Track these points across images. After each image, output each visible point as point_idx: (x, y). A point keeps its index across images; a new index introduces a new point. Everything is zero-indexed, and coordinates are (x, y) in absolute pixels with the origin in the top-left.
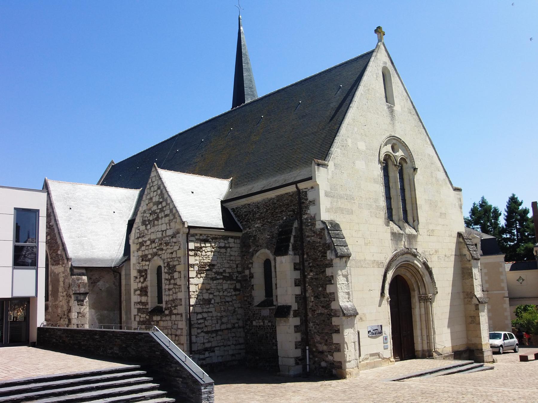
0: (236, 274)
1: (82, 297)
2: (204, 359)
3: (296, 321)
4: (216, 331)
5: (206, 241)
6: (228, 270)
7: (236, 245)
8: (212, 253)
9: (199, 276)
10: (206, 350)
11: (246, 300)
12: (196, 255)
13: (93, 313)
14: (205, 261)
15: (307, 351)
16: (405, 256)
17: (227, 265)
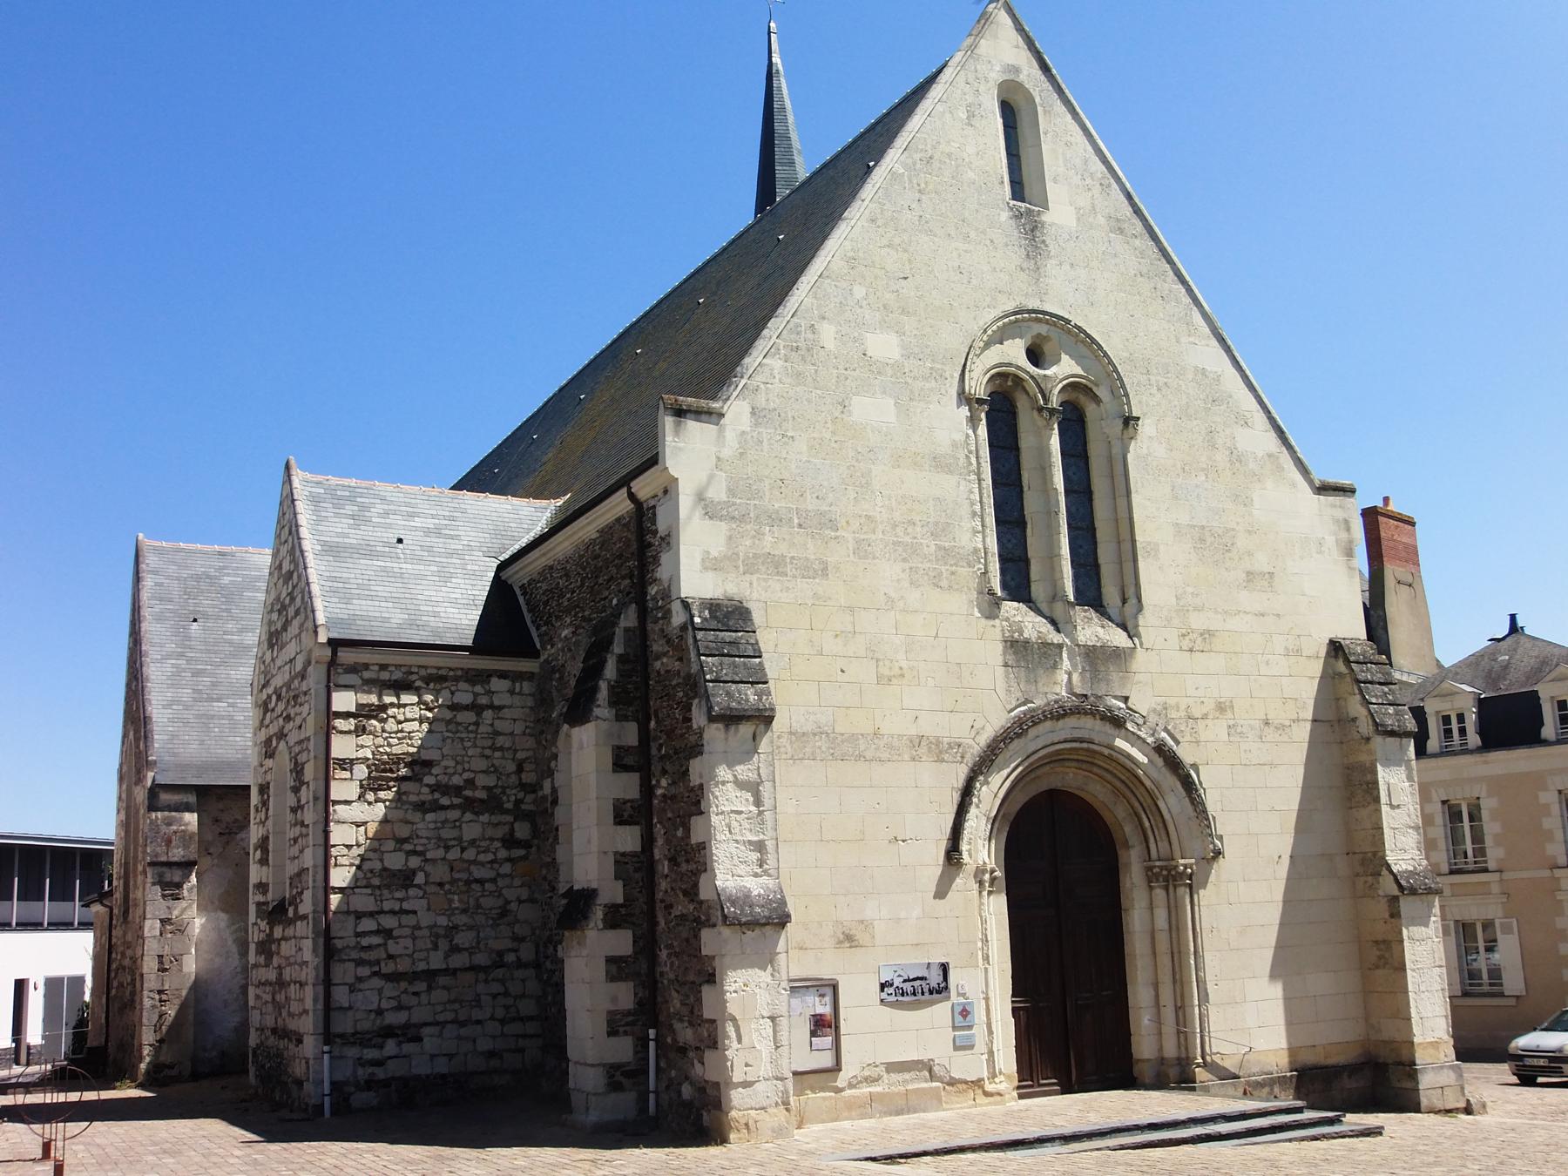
0: (514, 794)
1: (176, 876)
2: (379, 1063)
3: (621, 942)
4: (430, 975)
5: (399, 687)
6: (482, 780)
7: (517, 700)
8: (425, 727)
9: (370, 796)
10: (388, 1032)
11: (545, 878)
12: (360, 731)
13: (223, 925)
14: (397, 750)
15: (652, 1045)
16: (1071, 721)
17: (482, 764)
